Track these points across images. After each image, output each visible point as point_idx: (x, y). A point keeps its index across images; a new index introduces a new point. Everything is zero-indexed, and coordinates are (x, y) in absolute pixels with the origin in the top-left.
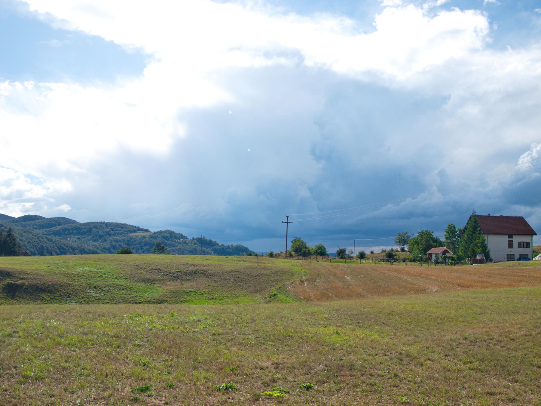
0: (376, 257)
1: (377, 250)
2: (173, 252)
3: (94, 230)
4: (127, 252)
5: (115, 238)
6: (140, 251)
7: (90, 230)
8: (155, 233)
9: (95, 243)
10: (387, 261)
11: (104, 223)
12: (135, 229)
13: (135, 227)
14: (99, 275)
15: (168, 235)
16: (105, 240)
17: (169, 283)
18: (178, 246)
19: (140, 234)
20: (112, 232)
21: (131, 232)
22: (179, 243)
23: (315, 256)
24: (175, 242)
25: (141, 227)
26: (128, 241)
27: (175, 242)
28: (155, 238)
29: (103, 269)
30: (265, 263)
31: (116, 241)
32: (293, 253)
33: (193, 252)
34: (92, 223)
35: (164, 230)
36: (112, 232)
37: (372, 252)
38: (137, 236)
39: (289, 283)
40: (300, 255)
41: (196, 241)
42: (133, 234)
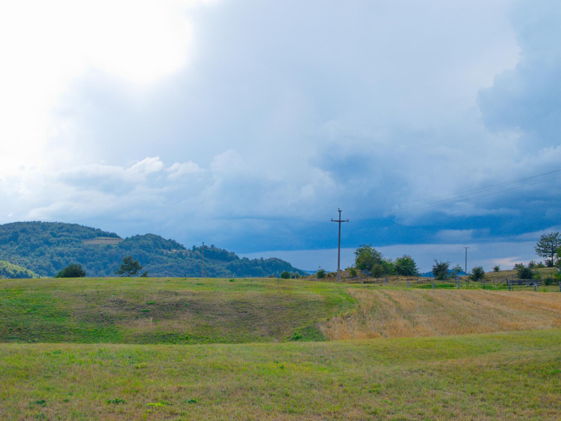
0: (502, 277)
1: (507, 264)
2: (159, 272)
3: (22, 236)
4: (74, 273)
5: (59, 249)
6: (102, 272)
7: (15, 238)
8: (127, 239)
9: (23, 259)
10: (520, 283)
11: (39, 223)
12: (92, 232)
13: (93, 229)
14: (25, 312)
15: (151, 243)
16: (42, 254)
17: (136, 322)
18: (166, 262)
19: (102, 242)
20: (53, 239)
21: (85, 238)
22: (170, 257)
23: (395, 277)
24: (162, 254)
25: (104, 229)
26: (82, 254)
27: (162, 254)
28: (128, 248)
29: (32, 301)
30: (291, 289)
31: (61, 255)
32: (358, 272)
33: (195, 272)
34: (19, 223)
35: (143, 233)
36: (53, 239)
37: (497, 269)
38: (96, 246)
39: (324, 319)
40: (371, 275)
41: (198, 252)
42: (90, 242)
